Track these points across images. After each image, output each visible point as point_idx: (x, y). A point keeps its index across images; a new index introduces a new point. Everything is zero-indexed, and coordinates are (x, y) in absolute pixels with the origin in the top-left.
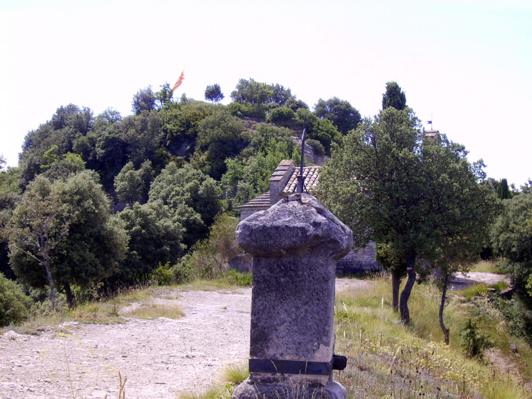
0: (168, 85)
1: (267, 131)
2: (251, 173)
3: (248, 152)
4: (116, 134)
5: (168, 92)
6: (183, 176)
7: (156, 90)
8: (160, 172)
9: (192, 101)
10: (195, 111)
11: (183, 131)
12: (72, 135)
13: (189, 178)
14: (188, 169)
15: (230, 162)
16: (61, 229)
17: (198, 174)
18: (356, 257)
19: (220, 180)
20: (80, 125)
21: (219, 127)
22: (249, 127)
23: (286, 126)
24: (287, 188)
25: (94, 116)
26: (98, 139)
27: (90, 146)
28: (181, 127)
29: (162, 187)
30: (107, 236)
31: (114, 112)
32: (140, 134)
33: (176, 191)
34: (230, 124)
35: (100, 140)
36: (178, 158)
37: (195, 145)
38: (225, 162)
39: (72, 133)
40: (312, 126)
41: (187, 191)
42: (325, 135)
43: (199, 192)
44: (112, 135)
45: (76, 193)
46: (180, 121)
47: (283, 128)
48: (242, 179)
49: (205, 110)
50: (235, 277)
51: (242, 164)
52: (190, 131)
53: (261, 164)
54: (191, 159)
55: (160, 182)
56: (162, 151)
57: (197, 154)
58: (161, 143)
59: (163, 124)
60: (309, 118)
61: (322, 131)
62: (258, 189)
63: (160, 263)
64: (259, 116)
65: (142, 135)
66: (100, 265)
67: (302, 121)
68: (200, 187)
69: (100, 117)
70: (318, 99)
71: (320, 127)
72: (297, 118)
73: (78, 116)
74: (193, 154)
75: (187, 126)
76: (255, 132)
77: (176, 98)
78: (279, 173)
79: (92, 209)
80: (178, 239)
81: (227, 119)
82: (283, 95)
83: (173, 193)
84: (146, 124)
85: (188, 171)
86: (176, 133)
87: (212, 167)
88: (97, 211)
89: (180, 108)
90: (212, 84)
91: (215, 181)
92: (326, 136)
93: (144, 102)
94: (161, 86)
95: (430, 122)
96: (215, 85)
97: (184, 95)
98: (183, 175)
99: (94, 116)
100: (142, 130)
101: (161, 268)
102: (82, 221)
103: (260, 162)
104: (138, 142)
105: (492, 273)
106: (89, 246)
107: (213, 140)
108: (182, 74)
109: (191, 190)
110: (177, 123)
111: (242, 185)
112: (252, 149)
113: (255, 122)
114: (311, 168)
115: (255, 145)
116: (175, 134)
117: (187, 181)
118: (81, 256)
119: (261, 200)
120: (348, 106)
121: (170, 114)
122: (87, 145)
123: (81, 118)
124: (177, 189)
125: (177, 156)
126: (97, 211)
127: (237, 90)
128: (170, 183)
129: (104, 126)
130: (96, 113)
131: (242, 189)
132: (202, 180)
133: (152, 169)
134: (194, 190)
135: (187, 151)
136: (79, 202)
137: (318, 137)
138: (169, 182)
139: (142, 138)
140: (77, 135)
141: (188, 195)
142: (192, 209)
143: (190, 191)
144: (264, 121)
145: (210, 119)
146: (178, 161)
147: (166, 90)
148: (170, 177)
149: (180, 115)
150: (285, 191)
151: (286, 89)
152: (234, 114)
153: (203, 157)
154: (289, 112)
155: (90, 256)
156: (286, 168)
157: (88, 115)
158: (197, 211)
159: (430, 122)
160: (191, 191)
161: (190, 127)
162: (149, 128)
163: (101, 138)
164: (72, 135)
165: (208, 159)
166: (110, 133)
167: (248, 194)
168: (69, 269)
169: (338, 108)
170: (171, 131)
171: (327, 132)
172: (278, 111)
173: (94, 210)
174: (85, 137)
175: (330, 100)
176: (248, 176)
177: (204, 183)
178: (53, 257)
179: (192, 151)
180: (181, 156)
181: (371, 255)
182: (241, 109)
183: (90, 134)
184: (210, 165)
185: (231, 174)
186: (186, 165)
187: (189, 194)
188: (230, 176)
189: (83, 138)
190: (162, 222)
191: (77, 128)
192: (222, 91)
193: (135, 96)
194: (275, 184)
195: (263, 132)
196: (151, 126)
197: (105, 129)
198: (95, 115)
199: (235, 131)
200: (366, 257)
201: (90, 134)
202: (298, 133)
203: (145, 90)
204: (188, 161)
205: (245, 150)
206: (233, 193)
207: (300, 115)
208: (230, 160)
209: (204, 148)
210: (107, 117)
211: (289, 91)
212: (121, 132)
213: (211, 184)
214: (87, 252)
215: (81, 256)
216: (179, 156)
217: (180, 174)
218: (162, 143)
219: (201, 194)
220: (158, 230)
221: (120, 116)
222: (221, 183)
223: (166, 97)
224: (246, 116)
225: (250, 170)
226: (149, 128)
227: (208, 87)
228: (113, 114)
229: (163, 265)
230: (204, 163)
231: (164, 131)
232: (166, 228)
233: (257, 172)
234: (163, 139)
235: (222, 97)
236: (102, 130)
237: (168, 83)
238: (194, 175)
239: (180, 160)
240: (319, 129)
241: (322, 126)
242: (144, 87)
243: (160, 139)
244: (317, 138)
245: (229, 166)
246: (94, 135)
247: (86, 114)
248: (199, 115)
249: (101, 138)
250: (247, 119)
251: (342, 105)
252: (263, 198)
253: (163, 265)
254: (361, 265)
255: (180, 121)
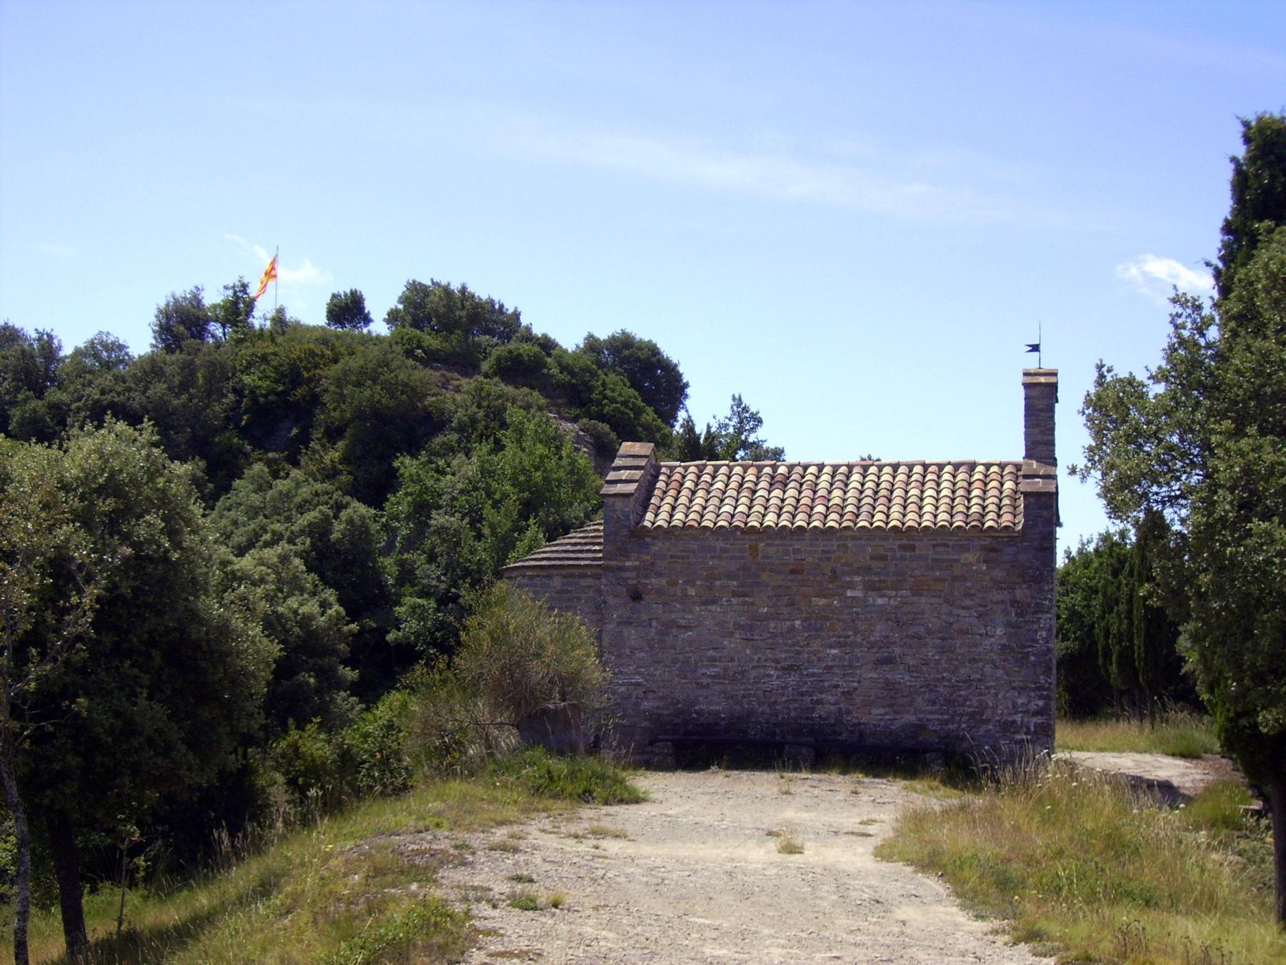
0: (244, 287)
1: (489, 395)
2: (462, 492)
3: (444, 443)
4: (119, 394)
5: (244, 302)
6: (287, 496)
7: (213, 297)
8: (227, 489)
9: (297, 326)
10: (312, 346)
11: (282, 392)
12: (7, 398)
13: (306, 501)
14: (297, 482)
15: (407, 465)
16: (66, 611)
17: (327, 493)
18: (849, 712)
19: (382, 509)
20: (28, 372)
21: (375, 383)
22: (445, 386)
23: (532, 388)
24: (649, 516)
25: (62, 354)
26: (74, 406)
27: (51, 424)
28: (276, 381)
29: (235, 523)
30: (208, 642)
31: (113, 343)
32: (177, 396)
33: (274, 532)
34: (402, 376)
35: (78, 409)
36: (271, 455)
37: (312, 427)
38: (396, 464)
39: (8, 392)
40: (591, 389)
41: (302, 532)
42: (620, 412)
43: (335, 536)
44: (109, 397)
45: (102, 491)
46: (275, 368)
47: (526, 390)
48: (440, 507)
49: (337, 344)
50: (543, 771)
51: (438, 471)
52: (300, 392)
53: (486, 472)
54: (303, 460)
55: (229, 510)
56: (229, 439)
57: (318, 447)
58: (227, 418)
59: (234, 374)
60: (582, 370)
61: (613, 401)
62: (486, 531)
63: (291, 721)
64: (465, 362)
65: (184, 397)
66: (183, 749)
67: (565, 377)
68: (336, 523)
69: (78, 352)
70: (586, 335)
71: (608, 392)
72: (555, 371)
73: (23, 351)
74: (307, 448)
75: (292, 382)
76: (458, 397)
77: (261, 317)
78: (624, 474)
79: (159, 546)
80: (335, 652)
81: (395, 363)
82: (503, 323)
83: (267, 537)
84: (193, 373)
85: (298, 486)
86: (265, 396)
87: (356, 479)
88: (175, 556)
89: (273, 340)
90: (344, 288)
91: (373, 511)
92: (623, 413)
93: (181, 323)
94: (226, 288)
95: (1035, 348)
96: (352, 293)
97: (281, 311)
98: (287, 496)
99: (62, 354)
100: (184, 387)
101: (294, 734)
102: (126, 591)
103: (487, 465)
104: (173, 414)
105: (1167, 754)
106: (146, 679)
107: (360, 415)
108: (273, 262)
109: (311, 530)
110: (269, 373)
111: (442, 520)
112: (454, 437)
113: (456, 375)
114: (705, 466)
115: (461, 429)
116: (262, 399)
117: (302, 508)
118: (117, 714)
119: (568, 547)
120: (654, 350)
121: (250, 351)
122: (43, 421)
123: (32, 357)
124: (277, 527)
125: (266, 451)
126: (175, 556)
127: (401, 307)
128: (256, 514)
129: (88, 376)
130: (70, 343)
131: (441, 531)
132: (339, 507)
133: (209, 481)
134: (320, 531)
135: (292, 439)
136: (114, 523)
137: (604, 416)
138: (254, 512)
139: (184, 406)
140: (20, 397)
141: (305, 543)
142: (316, 577)
143: (311, 532)
144: (479, 374)
145: (354, 363)
146: (269, 463)
147: (238, 298)
148: (256, 499)
149: (275, 354)
150: (647, 524)
151: (511, 311)
152: (409, 353)
153: (333, 455)
154: (535, 356)
155: (150, 713)
156: (643, 462)
157: (48, 346)
158: (327, 583)
159: (1035, 348)
160: (310, 534)
161: (300, 384)
162: (201, 381)
163: (80, 404)
164: (7, 398)
165: (345, 460)
166: (103, 392)
167: (458, 544)
168: (73, 761)
169: (631, 356)
170: (252, 392)
171: (625, 403)
172: (510, 352)
173: (167, 551)
174: (40, 403)
175: (613, 338)
176: (454, 499)
177: (344, 515)
178: (32, 726)
179: (305, 439)
180: (275, 451)
181: (891, 706)
182: (425, 344)
183: (54, 395)
184: (350, 473)
185: (411, 494)
186: (295, 473)
187: (308, 541)
188: (409, 498)
189: (34, 404)
190: (293, 602)
191: (21, 380)
192: (369, 306)
193: (161, 312)
194: (619, 503)
195: (479, 396)
196: (204, 377)
197: (90, 383)
198: (67, 351)
199: (416, 394)
200: (876, 711)
201: (53, 395)
202: (556, 405)
203: (185, 298)
204: (296, 464)
205: (438, 440)
206: (412, 543)
207: (560, 364)
208: (407, 461)
209: (333, 434)
210: (96, 356)
211: (516, 315)
212: (129, 390)
213: (362, 517)
214: (142, 701)
215: (117, 714)
216: (271, 451)
217: (281, 492)
218: (231, 417)
219: (338, 540)
220: (284, 626)
221: (127, 354)
222: (382, 516)
223: (239, 314)
224: (436, 361)
225: (460, 486)
226: (201, 381)
227: (334, 296)
228: (107, 347)
229: (300, 727)
230: (334, 468)
231: (235, 390)
232: (305, 621)
233: (476, 489)
234: (233, 409)
235: (367, 320)
236: (84, 385)
237: (246, 281)
238: (317, 494)
239: (275, 461)
240: (605, 397)
241: (613, 391)
242: (182, 289)
243: (225, 411)
244: (602, 418)
245: (407, 474)
246: (64, 397)
247: (43, 348)
248: (323, 356)
249: (80, 404)
250: (436, 369)
251: (640, 349)
252: (576, 544)
253: (300, 727)
254: (861, 734)
255: (275, 368)
